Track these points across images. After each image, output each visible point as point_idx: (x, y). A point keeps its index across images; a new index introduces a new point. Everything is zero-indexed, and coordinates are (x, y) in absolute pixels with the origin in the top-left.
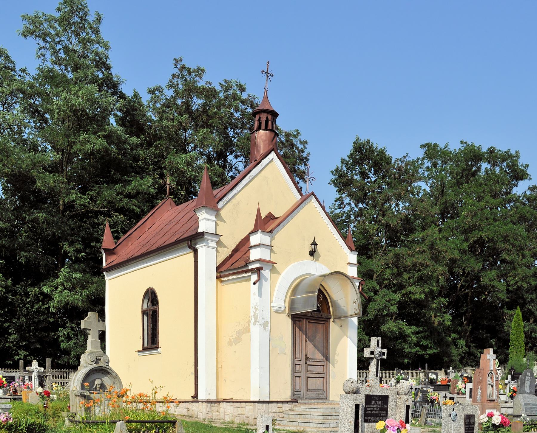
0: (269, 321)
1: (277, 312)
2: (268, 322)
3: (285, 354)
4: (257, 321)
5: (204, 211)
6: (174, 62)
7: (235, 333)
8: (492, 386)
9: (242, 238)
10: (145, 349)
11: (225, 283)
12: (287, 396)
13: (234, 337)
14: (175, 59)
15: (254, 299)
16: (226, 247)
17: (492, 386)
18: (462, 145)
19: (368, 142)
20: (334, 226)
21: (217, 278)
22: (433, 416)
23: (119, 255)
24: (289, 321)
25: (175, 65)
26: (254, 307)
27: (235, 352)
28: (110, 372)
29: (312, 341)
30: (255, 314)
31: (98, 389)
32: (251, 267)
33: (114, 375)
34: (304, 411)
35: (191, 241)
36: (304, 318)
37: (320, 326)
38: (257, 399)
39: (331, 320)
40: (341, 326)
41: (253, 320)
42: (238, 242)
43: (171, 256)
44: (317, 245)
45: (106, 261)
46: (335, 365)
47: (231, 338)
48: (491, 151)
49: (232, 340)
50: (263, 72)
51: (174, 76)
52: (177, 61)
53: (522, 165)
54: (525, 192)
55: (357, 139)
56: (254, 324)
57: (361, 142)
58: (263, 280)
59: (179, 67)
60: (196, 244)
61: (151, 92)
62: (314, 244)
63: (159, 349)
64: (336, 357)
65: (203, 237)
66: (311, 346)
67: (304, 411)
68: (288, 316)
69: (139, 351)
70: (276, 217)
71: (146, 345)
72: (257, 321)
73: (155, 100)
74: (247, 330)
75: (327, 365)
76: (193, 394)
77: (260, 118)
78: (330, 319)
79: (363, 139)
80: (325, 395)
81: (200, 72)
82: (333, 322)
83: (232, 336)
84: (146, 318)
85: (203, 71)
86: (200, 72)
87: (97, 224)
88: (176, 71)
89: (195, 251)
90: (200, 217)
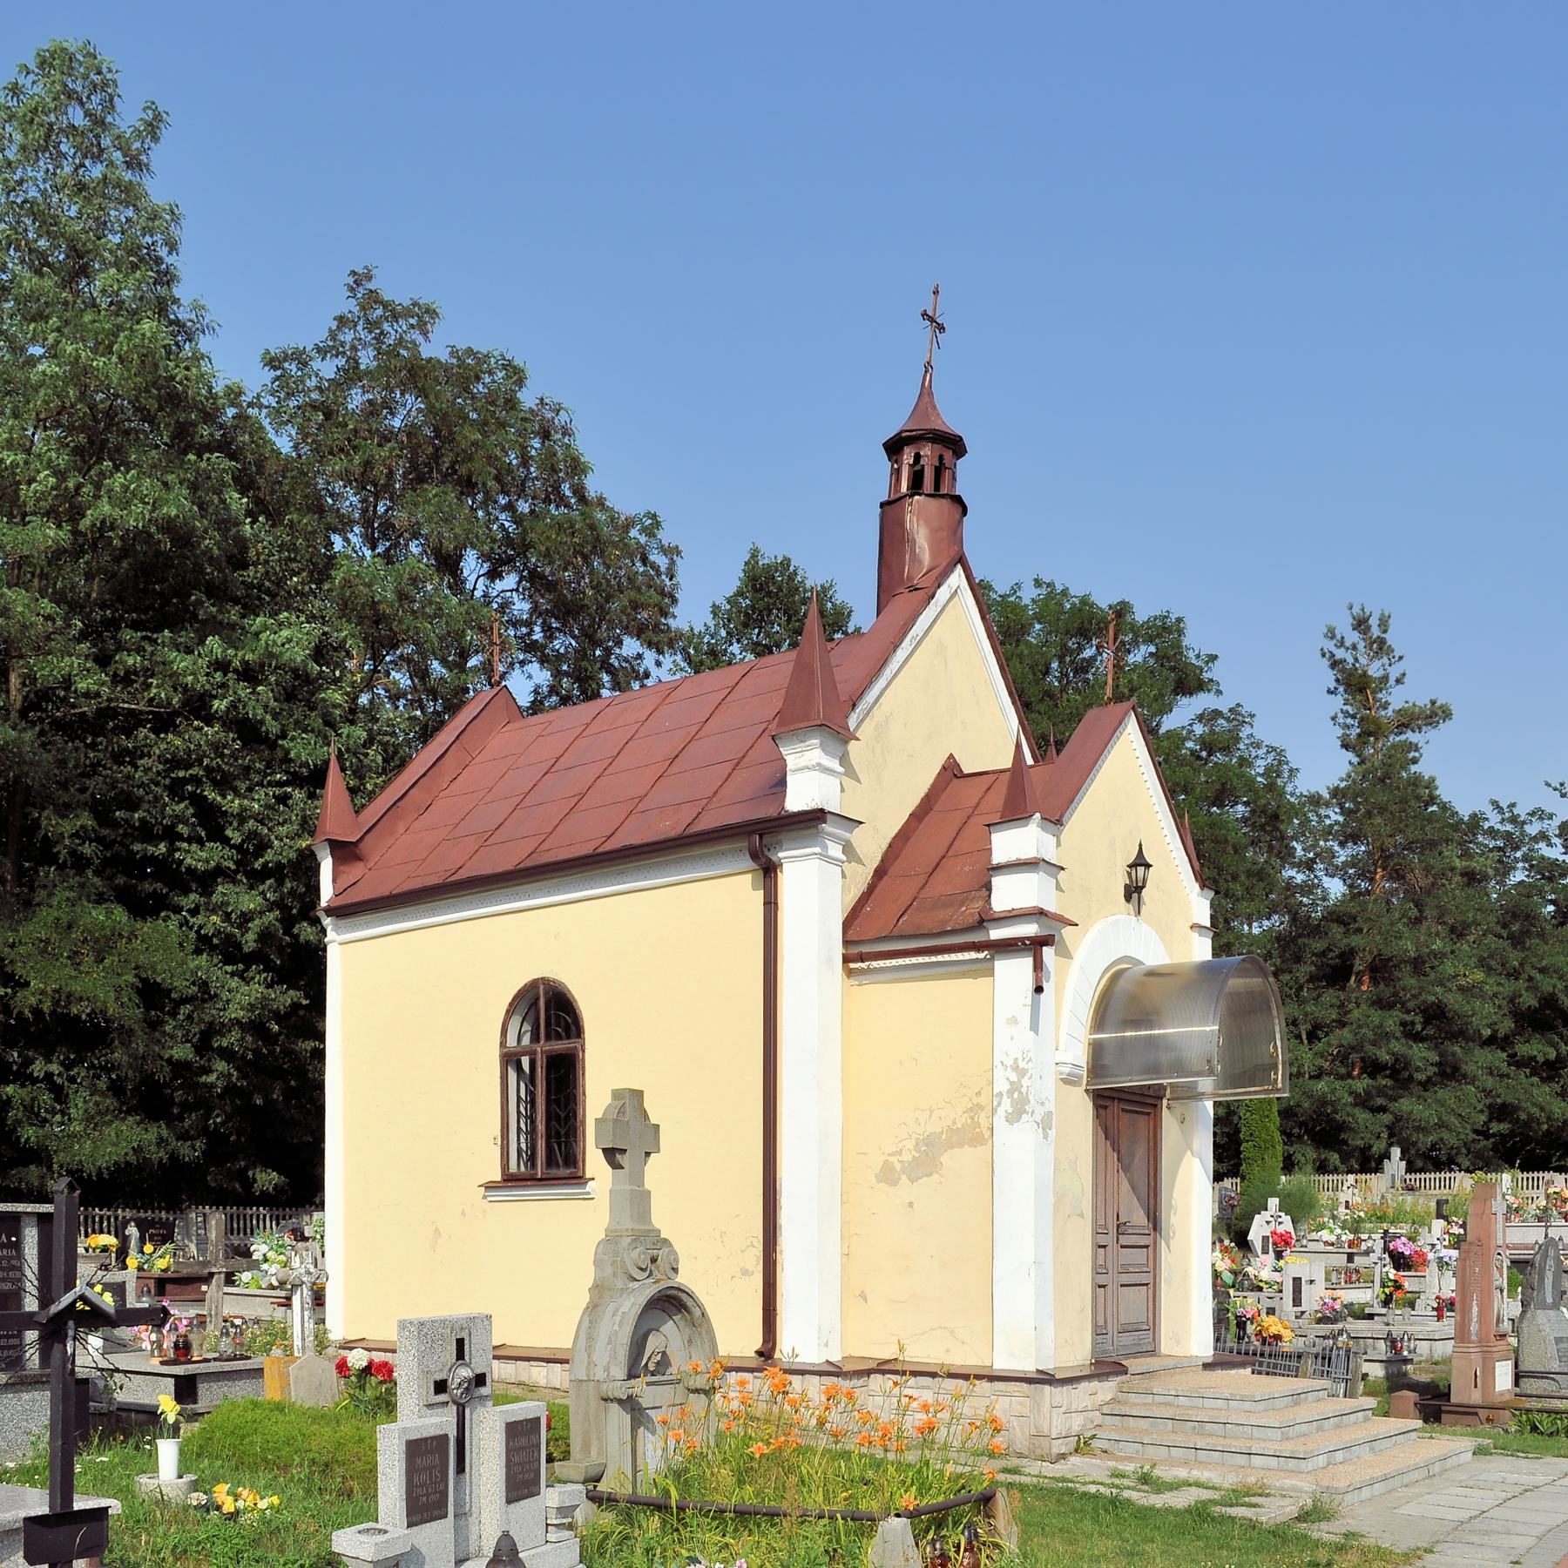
4: (1025, 1112)
5: (816, 741)
6: (351, 280)
7: (910, 1144)
8: (1502, 1291)
9: (893, 834)
10: (511, 1180)
11: (865, 979)
12: (1077, 1353)
13: (907, 1157)
14: (353, 273)
15: (1012, 1040)
16: (860, 861)
17: (1502, 1291)
18: (1039, 591)
19: (786, 563)
20: (1171, 810)
21: (846, 959)
22: (1264, 1369)
23: (370, 865)
24: (1087, 1106)
25: (352, 289)
26: (1009, 1062)
27: (911, 1205)
28: (690, 1303)
30: (1015, 1087)
31: (651, 1367)
32: (996, 934)
33: (697, 1312)
34: (1166, 1404)
35: (761, 836)
37: (1142, 1120)
38: (1029, 1366)
39: (1165, 1102)
41: (1006, 1105)
42: (884, 846)
43: (646, 879)
44: (1148, 866)
45: (334, 881)
47: (893, 1159)
48: (1122, 610)
49: (898, 1166)
50: (924, 314)
51: (342, 321)
52: (359, 279)
53: (1198, 656)
54: (1191, 725)
55: (755, 554)
56: (1015, 1117)
57: (766, 561)
59: (361, 292)
60: (779, 846)
61: (272, 362)
63: (590, 1183)
64: (1173, 1220)
65: (816, 827)
67: (1166, 1404)
68: (1087, 1091)
69: (490, 1187)
70: (966, 771)
71: (513, 1168)
72: (1025, 1112)
73: (285, 386)
74: (975, 1135)
75: (1155, 1243)
76: (757, 1342)
77: (917, 457)
79: (771, 554)
81: (424, 316)
82: (1169, 1108)
83: (900, 1153)
85: (432, 313)
86: (424, 316)
87: (127, 751)
88: (350, 307)
89: (769, 872)
90: (792, 761)
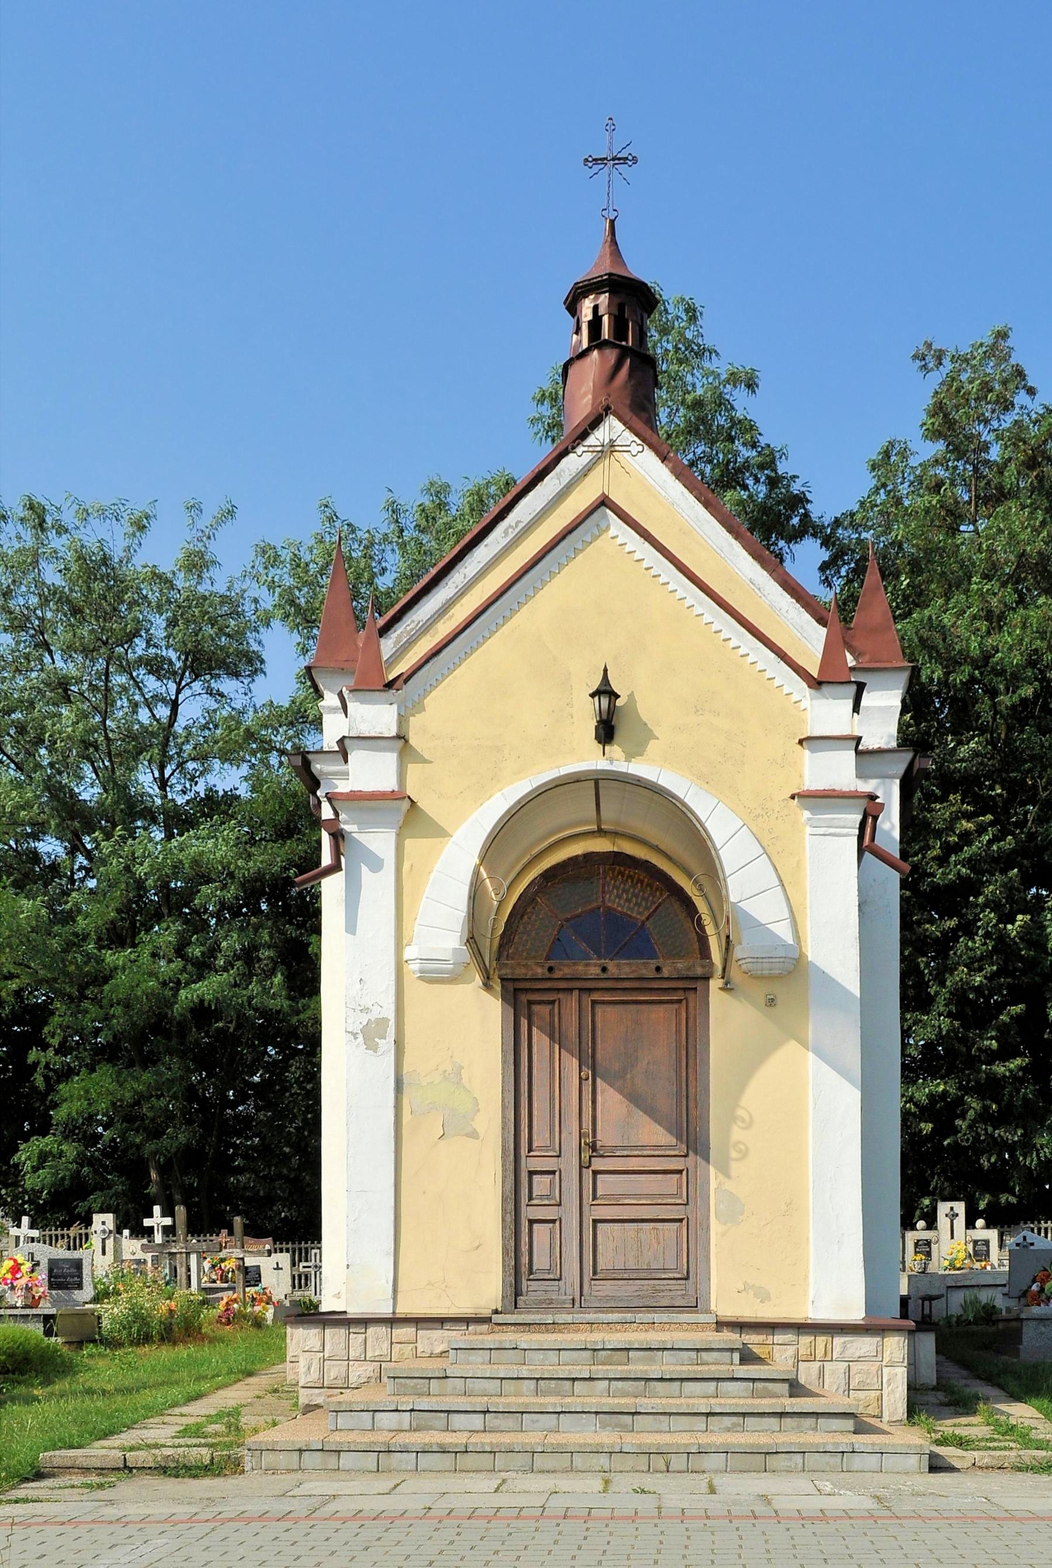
0: (392, 1017)
1: (431, 977)
2: (385, 1020)
3: (474, 1135)
29: (617, 1080)
36: (571, 990)
37: (659, 1013)
39: (715, 984)
40: (771, 1002)
46: (734, 1165)
58: (364, 869)
62: (605, 691)
64: (737, 1134)
66: (610, 1099)
78: (706, 978)
80: (691, 1292)
84: (526, 1021)
